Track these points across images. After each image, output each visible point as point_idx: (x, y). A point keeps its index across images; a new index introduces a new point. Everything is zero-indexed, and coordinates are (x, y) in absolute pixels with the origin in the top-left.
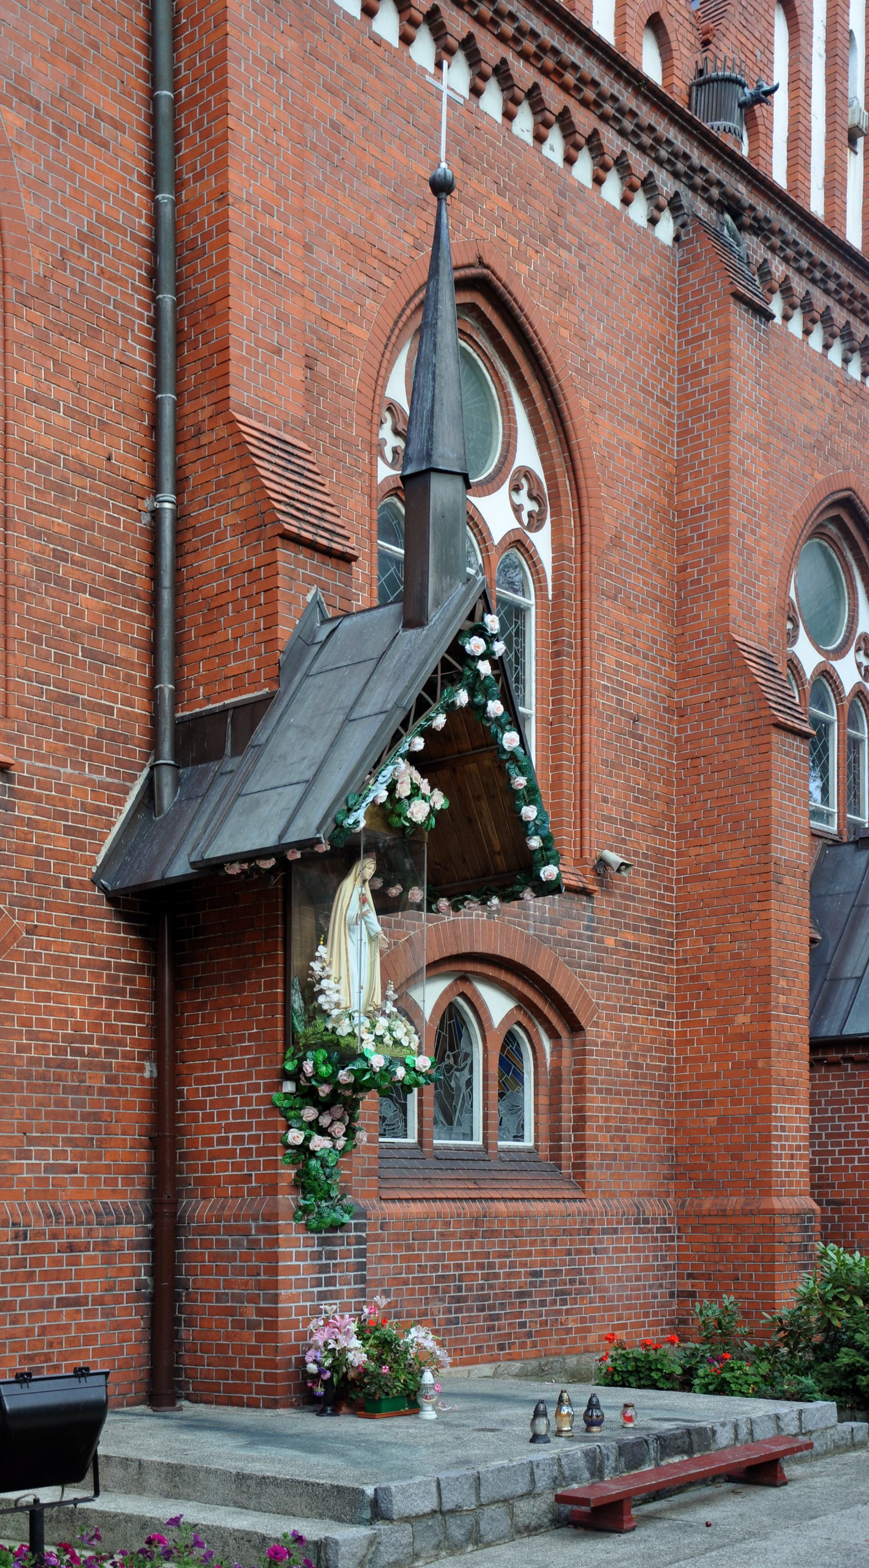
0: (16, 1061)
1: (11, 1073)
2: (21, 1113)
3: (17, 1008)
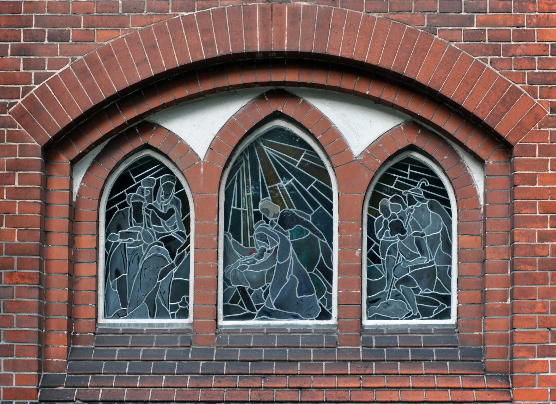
0: (538, 251)
1: (532, 264)
2: (545, 306)
3: (540, 194)
